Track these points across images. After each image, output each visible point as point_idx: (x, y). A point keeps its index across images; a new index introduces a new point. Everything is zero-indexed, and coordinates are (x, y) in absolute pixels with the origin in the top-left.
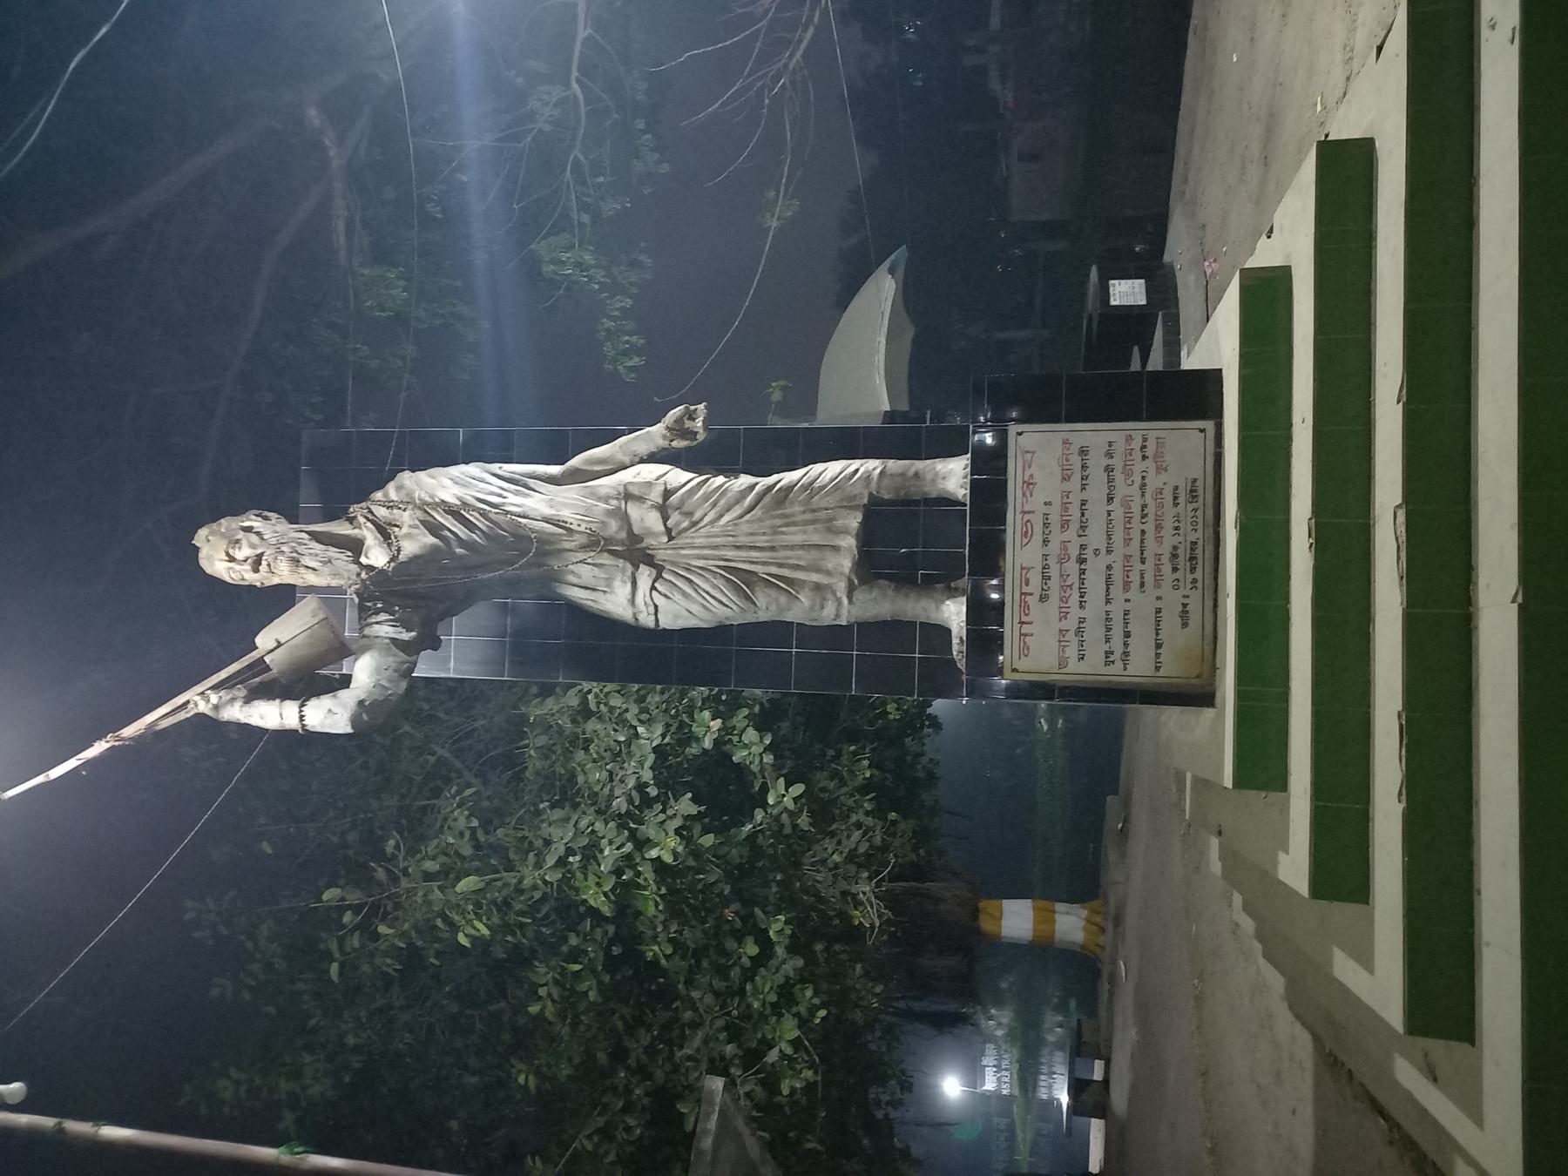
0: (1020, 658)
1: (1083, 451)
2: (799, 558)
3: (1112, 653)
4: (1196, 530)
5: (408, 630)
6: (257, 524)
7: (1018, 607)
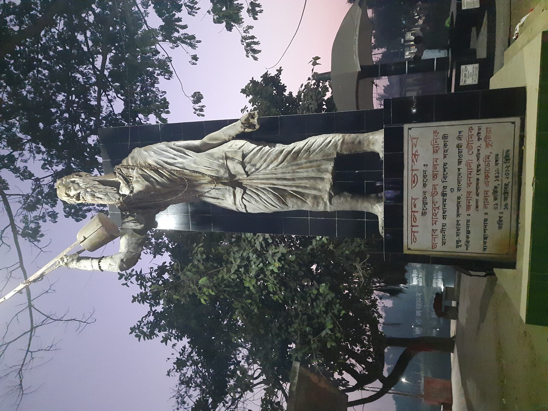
1: (445, 137)
2: (306, 183)
3: (460, 241)
4: (508, 178)
5: (141, 224)
6: (77, 179)
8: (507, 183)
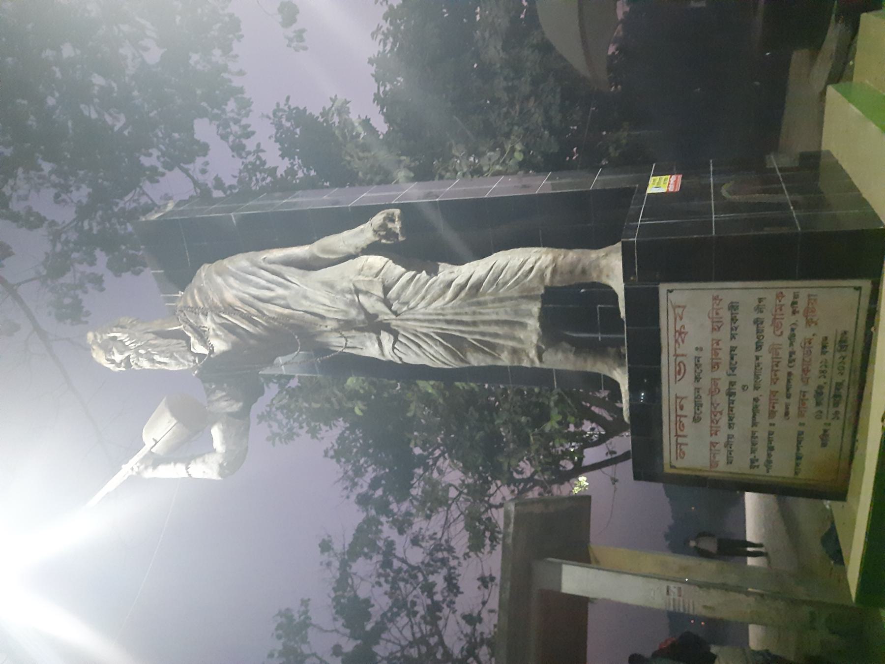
0: (677, 459)
1: (733, 306)
3: (757, 460)
6: (119, 335)
7: (674, 426)
8: (840, 381)
